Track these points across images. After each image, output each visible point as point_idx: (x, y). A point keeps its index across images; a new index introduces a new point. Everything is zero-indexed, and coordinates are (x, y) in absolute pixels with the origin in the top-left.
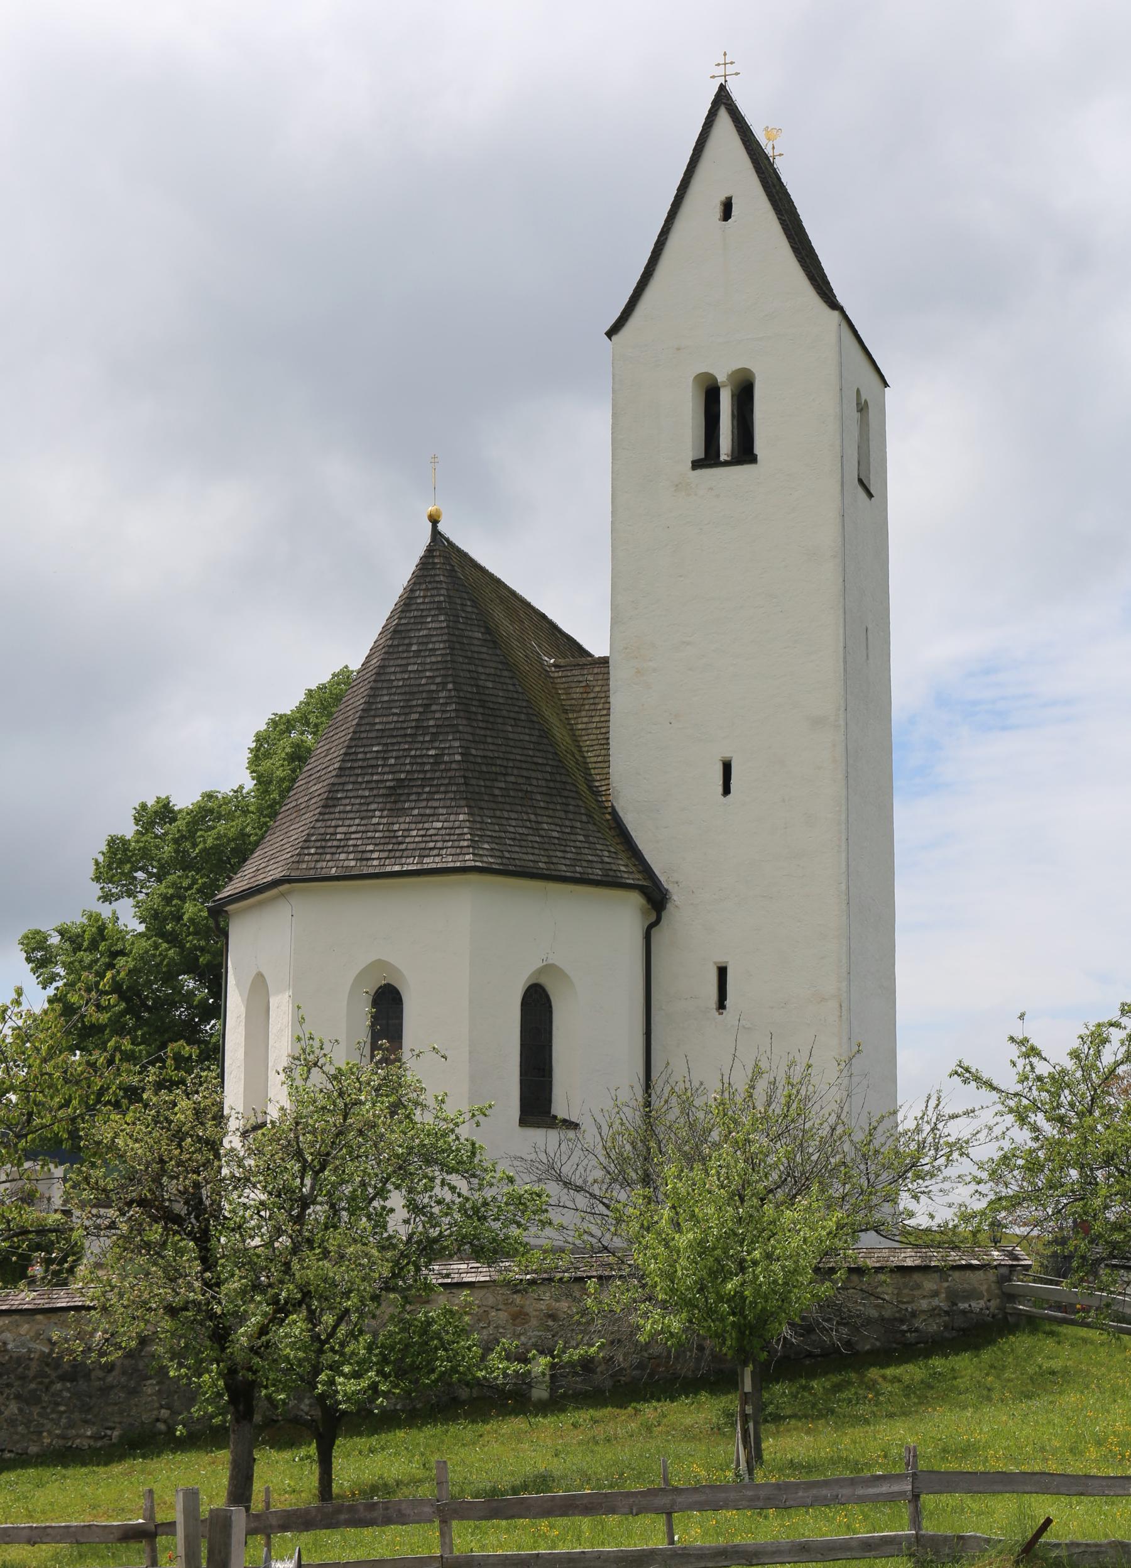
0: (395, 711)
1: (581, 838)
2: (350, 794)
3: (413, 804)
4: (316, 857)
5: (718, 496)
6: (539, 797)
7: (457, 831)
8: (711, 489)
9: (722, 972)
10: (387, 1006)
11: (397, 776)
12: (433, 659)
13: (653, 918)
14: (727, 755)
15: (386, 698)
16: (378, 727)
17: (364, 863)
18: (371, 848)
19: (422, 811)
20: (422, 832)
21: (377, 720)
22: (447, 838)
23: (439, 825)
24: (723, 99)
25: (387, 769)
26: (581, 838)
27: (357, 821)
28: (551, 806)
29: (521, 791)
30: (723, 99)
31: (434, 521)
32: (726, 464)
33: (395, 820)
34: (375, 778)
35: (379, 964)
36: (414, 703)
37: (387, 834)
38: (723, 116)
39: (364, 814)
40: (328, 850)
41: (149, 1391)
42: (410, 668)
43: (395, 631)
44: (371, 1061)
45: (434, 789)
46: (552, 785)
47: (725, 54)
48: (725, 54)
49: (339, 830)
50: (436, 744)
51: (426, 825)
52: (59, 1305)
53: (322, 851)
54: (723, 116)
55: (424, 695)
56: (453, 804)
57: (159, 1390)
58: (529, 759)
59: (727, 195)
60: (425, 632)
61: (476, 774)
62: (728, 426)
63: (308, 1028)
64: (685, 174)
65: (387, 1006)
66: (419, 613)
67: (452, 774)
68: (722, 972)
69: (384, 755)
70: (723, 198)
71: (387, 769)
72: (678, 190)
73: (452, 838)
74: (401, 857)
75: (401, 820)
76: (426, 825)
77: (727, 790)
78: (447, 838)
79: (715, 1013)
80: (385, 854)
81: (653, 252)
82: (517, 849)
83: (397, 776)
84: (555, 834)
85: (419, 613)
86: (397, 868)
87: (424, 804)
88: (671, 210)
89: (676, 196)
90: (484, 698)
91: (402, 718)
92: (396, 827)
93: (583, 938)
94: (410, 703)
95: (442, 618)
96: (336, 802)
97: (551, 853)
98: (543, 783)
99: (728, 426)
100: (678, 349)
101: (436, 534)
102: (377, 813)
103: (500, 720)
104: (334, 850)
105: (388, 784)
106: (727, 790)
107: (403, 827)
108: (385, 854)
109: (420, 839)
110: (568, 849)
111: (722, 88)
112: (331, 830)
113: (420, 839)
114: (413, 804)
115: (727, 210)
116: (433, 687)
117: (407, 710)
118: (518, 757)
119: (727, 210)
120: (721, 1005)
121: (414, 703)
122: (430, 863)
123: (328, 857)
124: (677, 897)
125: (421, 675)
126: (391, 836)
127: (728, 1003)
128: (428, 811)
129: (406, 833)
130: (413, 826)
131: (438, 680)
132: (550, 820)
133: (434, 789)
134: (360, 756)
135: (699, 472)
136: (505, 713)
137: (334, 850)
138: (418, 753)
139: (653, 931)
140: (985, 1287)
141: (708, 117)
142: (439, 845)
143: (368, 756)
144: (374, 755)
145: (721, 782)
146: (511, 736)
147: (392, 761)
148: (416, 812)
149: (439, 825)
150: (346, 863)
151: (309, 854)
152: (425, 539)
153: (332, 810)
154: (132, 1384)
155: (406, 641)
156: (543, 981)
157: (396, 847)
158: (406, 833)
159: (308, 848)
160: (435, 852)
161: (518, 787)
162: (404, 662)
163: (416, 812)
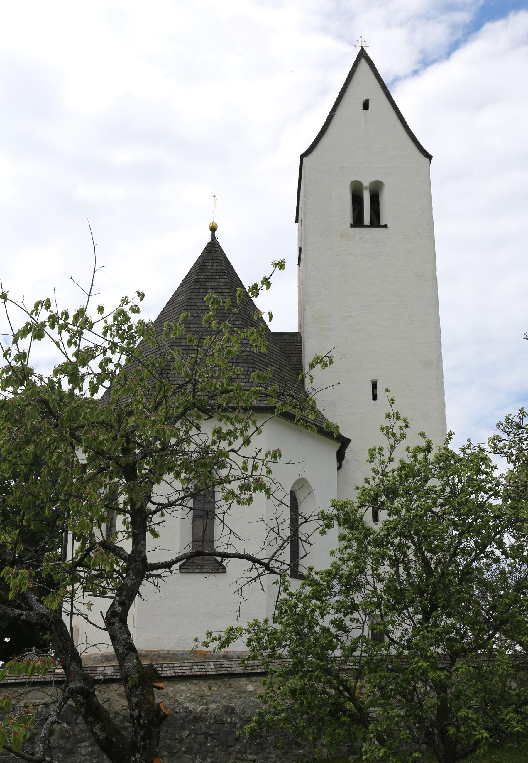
5: (366, 242)
8: (362, 238)
14: (375, 378)
21: (191, 326)
24: (363, 55)
29: (280, 375)
30: (363, 55)
31: (213, 229)
38: (363, 63)
41: (83, 752)
43: (196, 282)
47: (361, 37)
52: (9, 681)
54: (363, 63)
57: (91, 751)
59: (367, 98)
60: (216, 283)
63: (396, 408)
64: (344, 85)
66: (210, 274)
70: (364, 100)
85: (210, 274)
95: (225, 277)
99: (366, 207)
100: (342, 168)
101: (213, 238)
115: (366, 106)
119: (366, 106)
135: (354, 229)
140: (130, 737)
152: (209, 240)
154: (69, 746)
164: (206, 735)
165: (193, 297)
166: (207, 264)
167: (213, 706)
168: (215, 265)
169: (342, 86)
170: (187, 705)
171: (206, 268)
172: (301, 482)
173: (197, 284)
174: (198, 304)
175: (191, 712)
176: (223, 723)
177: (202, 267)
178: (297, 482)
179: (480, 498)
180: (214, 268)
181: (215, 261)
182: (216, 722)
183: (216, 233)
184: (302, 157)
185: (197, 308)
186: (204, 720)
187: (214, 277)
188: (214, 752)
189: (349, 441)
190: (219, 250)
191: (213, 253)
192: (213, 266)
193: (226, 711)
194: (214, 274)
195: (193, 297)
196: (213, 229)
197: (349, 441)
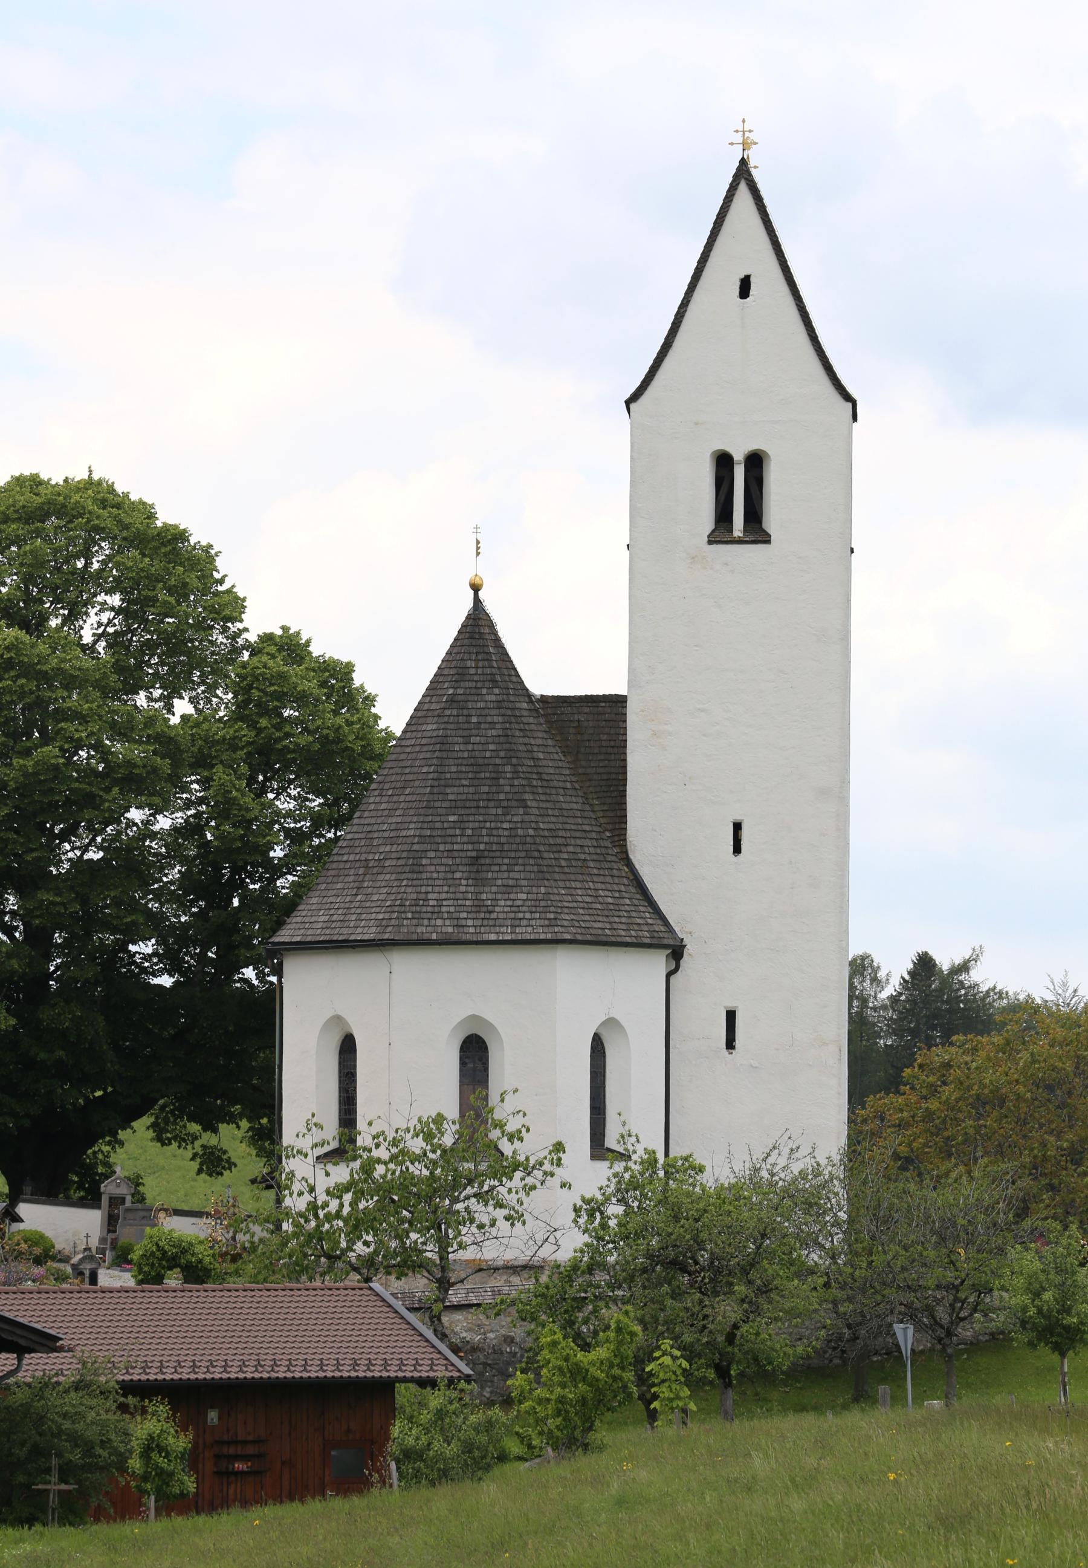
0: (464, 782)
1: (628, 902)
2: (435, 862)
3: (495, 875)
4: (414, 922)
6: (591, 864)
7: (542, 903)
9: (731, 1016)
10: (474, 1052)
11: (476, 846)
12: (494, 732)
13: (673, 966)
15: (454, 769)
16: (451, 797)
17: (461, 929)
18: (464, 915)
19: (505, 882)
20: (509, 903)
21: (448, 791)
22: (534, 909)
23: (524, 896)
24: (743, 173)
25: (465, 839)
26: (628, 902)
27: (446, 889)
28: (602, 872)
30: (743, 173)
31: (476, 588)
32: (740, 542)
33: (481, 889)
34: (456, 847)
35: (475, 1018)
36: (482, 775)
37: (476, 903)
38: (743, 187)
39: (451, 882)
40: (425, 915)
42: (472, 740)
44: (637, 1136)
45: (513, 862)
46: (598, 851)
47: (744, 121)
48: (744, 121)
49: (430, 896)
50: (509, 818)
51: (512, 896)
53: (418, 917)
54: (743, 187)
55: (491, 768)
56: (533, 876)
58: (580, 827)
60: (483, 705)
61: (547, 848)
62: (740, 500)
65: (474, 1052)
67: (528, 847)
68: (731, 1016)
69: (461, 824)
71: (465, 839)
72: (699, 262)
73: (538, 909)
74: (495, 926)
75: (487, 889)
76: (512, 896)
77: (737, 849)
78: (534, 909)
79: (725, 1052)
80: (479, 923)
81: (673, 323)
82: (587, 918)
83: (476, 846)
84: (610, 900)
86: (493, 937)
87: (506, 875)
88: (691, 283)
89: (697, 268)
90: (540, 770)
91: (472, 790)
92: (484, 896)
93: (615, 988)
94: (478, 776)
95: (497, 691)
96: (421, 869)
97: (612, 919)
98: (592, 850)
99: (740, 500)
100: (696, 424)
102: (464, 882)
103: (553, 791)
104: (429, 915)
105: (469, 854)
106: (737, 849)
107: (490, 896)
108: (479, 923)
109: (508, 909)
110: (621, 914)
111: (743, 162)
112: (423, 896)
113: (508, 909)
114: (495, 875)
115: (745, 288)
116: (498, 761)
117: (476, 782)
118: (573, 827)
119: (745, 288)
120: (730, 1044)
121: (482, 775)
122: (522, 933)
123: (426, 922)
124: (690, 949)
125: (485, 747)
126: (478, 906)
127: (738, 1043)
128: (511, 882)
129: (494, 903)
130: (499, 896)
131: (502, 754)
132: (603, 886)
133: (513, 862)
134: (438, 825)
136: (556, 783)
137: (429, 915)
138: (493, 825)
139: (672, 979)
141: (729, 191)
142: (528, 915)
143: (445, 825)
144: (451, 825)
145: (732, 843)
146: (564, 806)
147: (470, 832)
148: (499, 882)
149: (524, 896)
150: (444, 929)
151: (407, 919)
152: (469, 604)
153: (420, 876)
155: (465, 712)
156: (599, 1031)
157: (487, 916)
158: (494, 903)
159: (404, 912)
160: (525, 922)
161: (576, 857)
162: (465, 733)
163: (499, 882)
164: (485, 1364)
165: (449, 732)
166: (469, 664)
167: (491, 1335)
168: (481, 664)
169: (702, 249)
170: (464, 1335)
171: (466, 671)
172: (611, 1023)
173: (454, 705)
174: (457, 748)
175: (468, 1342)
176: (502, 1353)
177: (460, 671)
178: (604, 1023)
179: (453, 1407)
180: (480, 671)
181: (480, 657)
182: (495, 1352)
183: (481, 594)
184: (628, 403)
185: (455, 755)
186: (481, 1350)
187: (479, 692)
188: (492, 1381)
189: (594, 1157)
190: (487, 630)
191: (478, 636)
192: (477, 668)
193: (505, 1340)
194: (479, 685)
195: (449, 732)
196: (476, 588)
197: (594, 1157)
